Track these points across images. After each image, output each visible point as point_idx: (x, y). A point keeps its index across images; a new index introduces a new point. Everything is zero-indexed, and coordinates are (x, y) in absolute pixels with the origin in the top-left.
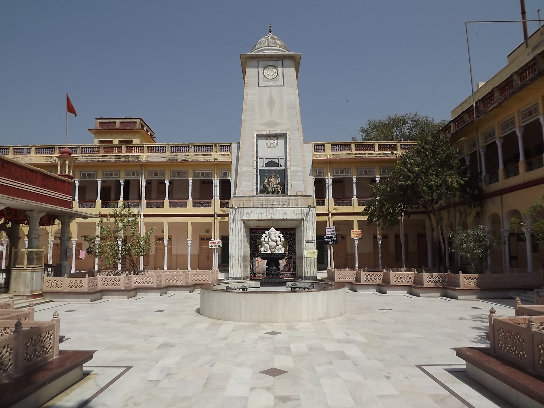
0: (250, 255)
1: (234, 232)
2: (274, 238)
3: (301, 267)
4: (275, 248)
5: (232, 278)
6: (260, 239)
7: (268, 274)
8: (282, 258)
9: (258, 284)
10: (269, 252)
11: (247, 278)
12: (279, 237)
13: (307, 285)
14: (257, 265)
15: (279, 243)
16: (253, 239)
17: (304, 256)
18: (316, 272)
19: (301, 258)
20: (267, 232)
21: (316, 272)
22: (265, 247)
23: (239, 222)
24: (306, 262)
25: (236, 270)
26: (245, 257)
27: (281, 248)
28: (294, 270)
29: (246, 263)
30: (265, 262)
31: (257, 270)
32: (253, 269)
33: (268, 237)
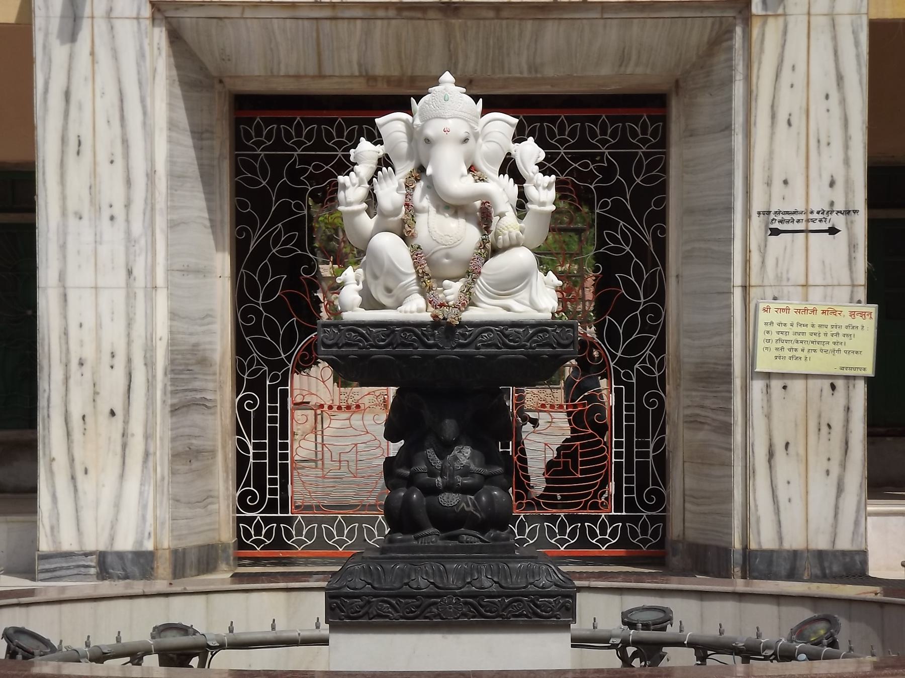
0: (241, 348)
1: (80, 126)
2: (459, 184)
3: (716, 460)
4: (471, 273)
5: (65, 562)
6: (328, 195)
7: (400, 518)
8: (539, 370)
9: (317, 603)
10: (415, 309)
11: (207, 559)
12: (509, 167)
13: (769, 624)
14: (301, 447)
15: (508, 223)
16: (261, 200)
17: (750, 356)
18: (861, 516)
19: (716, 377)
20: (392, 125)
21: (861, 516)
22: (380, 270)
23: (126, 31)
24: (764, 420)
25: (99, 487)
26: (185, 363)
27: (521, 279)
28: (649, 483)
29: (196, 417)
30: (376, 401)
31: (297, 491)
32: (262, 475)
33: (405, 168)
